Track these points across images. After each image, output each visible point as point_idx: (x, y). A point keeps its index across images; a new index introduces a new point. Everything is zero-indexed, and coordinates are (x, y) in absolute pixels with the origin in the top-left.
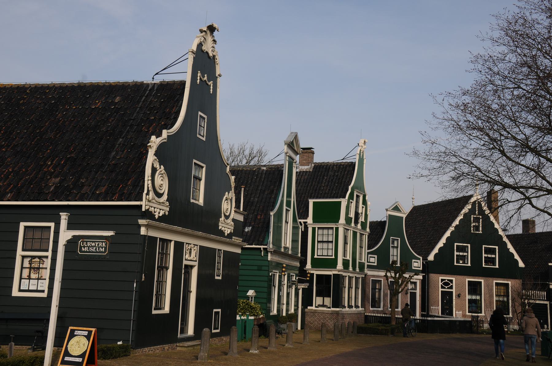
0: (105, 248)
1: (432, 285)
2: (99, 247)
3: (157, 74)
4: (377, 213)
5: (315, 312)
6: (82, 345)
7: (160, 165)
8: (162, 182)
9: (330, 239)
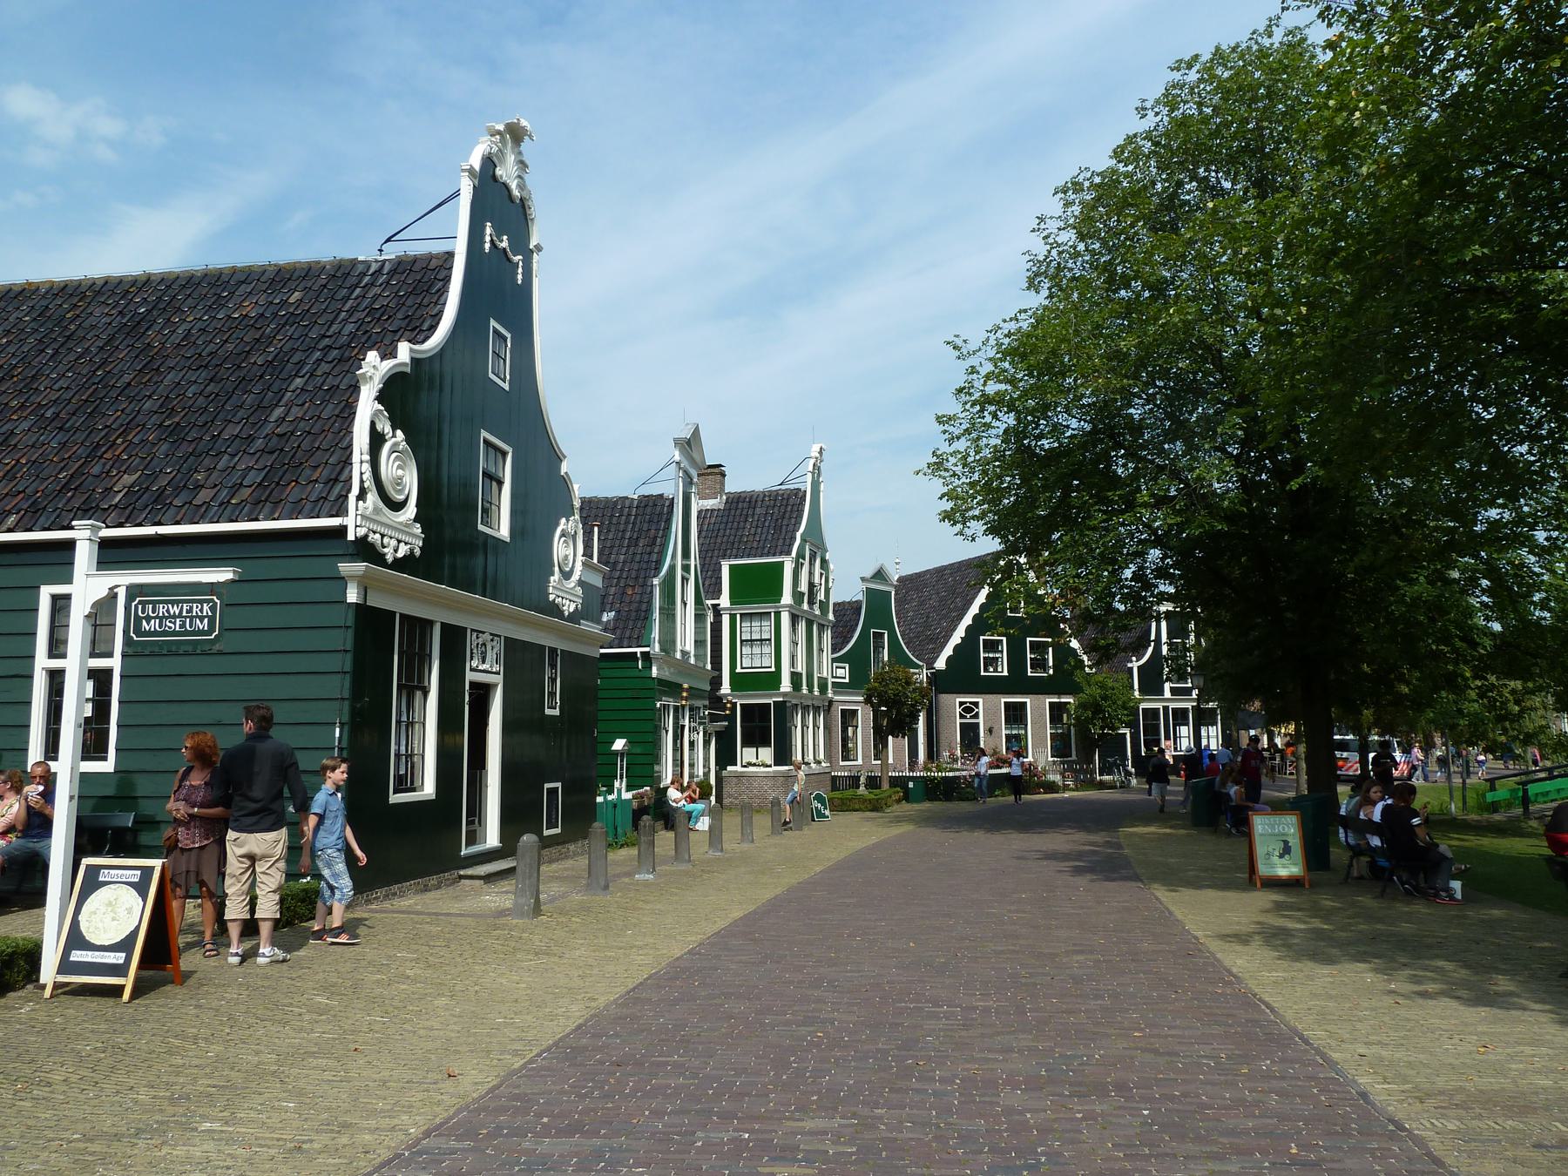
0: (212, 620)
1: (943, 712)
2: (191, 618)
3: (388, 240)
4: (846, 587)
5: (739, 776)
6: (122, 912)
7: (394, 429)
8: (404, 476)
9: (747, 650)
